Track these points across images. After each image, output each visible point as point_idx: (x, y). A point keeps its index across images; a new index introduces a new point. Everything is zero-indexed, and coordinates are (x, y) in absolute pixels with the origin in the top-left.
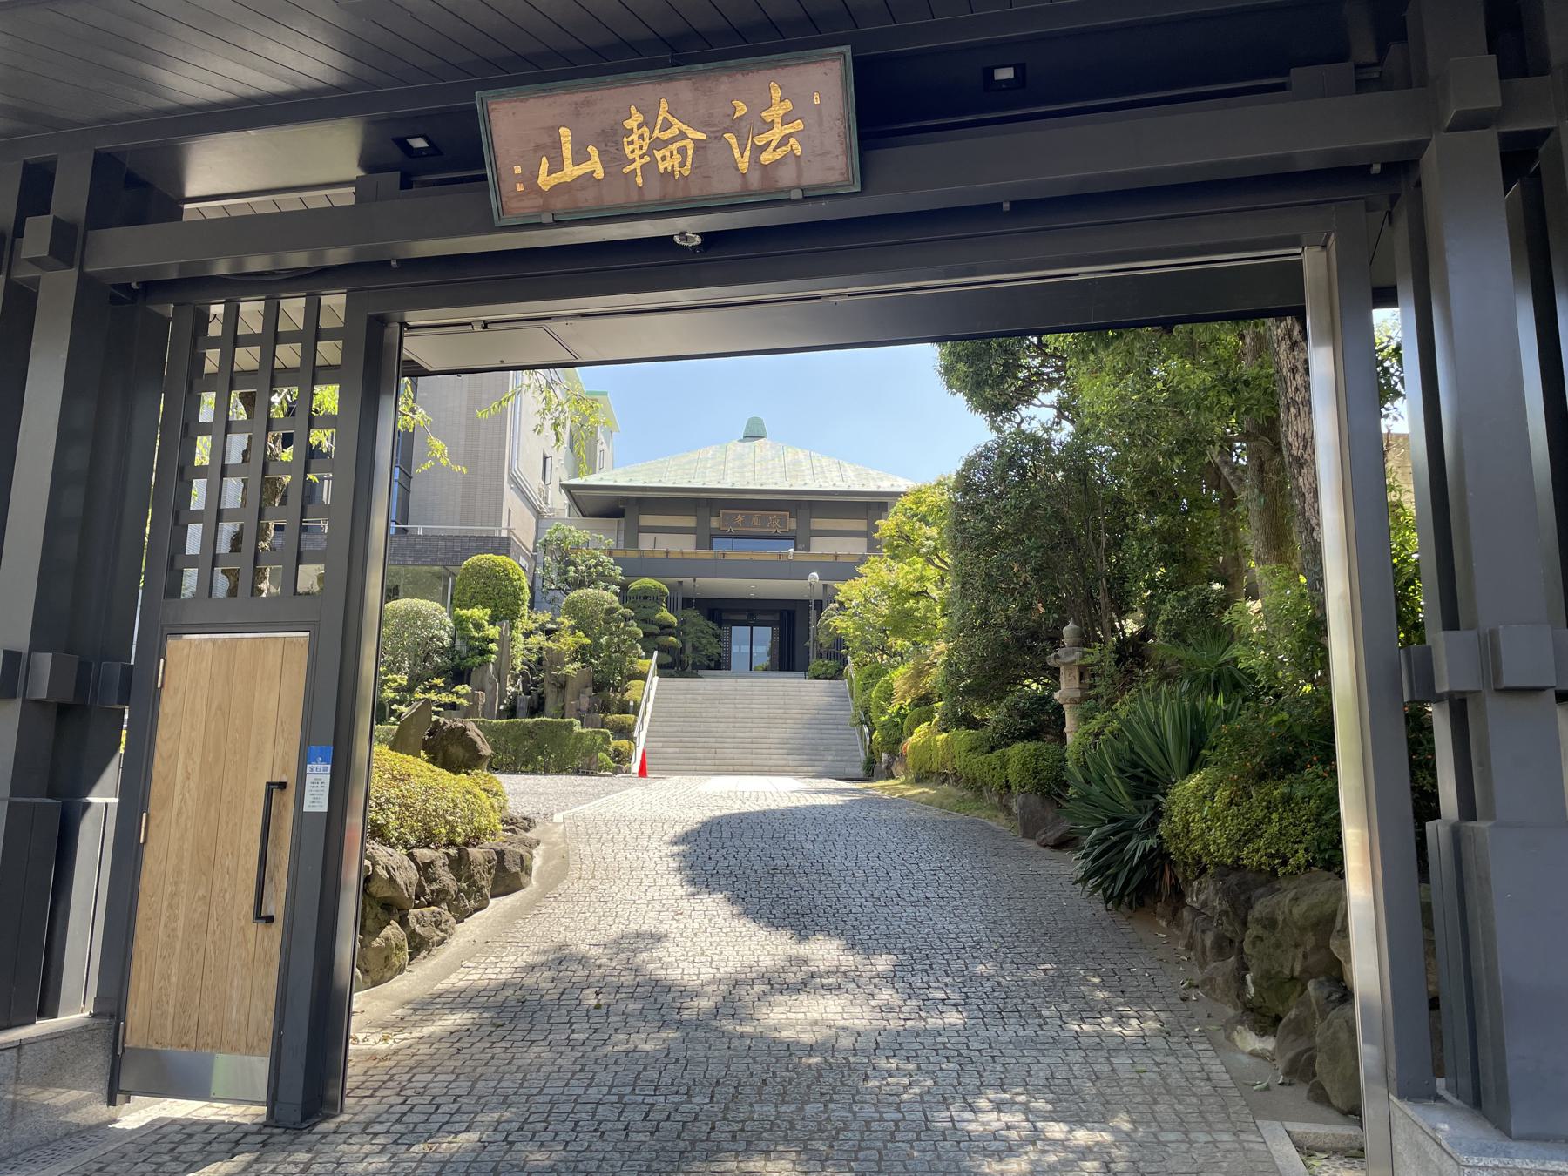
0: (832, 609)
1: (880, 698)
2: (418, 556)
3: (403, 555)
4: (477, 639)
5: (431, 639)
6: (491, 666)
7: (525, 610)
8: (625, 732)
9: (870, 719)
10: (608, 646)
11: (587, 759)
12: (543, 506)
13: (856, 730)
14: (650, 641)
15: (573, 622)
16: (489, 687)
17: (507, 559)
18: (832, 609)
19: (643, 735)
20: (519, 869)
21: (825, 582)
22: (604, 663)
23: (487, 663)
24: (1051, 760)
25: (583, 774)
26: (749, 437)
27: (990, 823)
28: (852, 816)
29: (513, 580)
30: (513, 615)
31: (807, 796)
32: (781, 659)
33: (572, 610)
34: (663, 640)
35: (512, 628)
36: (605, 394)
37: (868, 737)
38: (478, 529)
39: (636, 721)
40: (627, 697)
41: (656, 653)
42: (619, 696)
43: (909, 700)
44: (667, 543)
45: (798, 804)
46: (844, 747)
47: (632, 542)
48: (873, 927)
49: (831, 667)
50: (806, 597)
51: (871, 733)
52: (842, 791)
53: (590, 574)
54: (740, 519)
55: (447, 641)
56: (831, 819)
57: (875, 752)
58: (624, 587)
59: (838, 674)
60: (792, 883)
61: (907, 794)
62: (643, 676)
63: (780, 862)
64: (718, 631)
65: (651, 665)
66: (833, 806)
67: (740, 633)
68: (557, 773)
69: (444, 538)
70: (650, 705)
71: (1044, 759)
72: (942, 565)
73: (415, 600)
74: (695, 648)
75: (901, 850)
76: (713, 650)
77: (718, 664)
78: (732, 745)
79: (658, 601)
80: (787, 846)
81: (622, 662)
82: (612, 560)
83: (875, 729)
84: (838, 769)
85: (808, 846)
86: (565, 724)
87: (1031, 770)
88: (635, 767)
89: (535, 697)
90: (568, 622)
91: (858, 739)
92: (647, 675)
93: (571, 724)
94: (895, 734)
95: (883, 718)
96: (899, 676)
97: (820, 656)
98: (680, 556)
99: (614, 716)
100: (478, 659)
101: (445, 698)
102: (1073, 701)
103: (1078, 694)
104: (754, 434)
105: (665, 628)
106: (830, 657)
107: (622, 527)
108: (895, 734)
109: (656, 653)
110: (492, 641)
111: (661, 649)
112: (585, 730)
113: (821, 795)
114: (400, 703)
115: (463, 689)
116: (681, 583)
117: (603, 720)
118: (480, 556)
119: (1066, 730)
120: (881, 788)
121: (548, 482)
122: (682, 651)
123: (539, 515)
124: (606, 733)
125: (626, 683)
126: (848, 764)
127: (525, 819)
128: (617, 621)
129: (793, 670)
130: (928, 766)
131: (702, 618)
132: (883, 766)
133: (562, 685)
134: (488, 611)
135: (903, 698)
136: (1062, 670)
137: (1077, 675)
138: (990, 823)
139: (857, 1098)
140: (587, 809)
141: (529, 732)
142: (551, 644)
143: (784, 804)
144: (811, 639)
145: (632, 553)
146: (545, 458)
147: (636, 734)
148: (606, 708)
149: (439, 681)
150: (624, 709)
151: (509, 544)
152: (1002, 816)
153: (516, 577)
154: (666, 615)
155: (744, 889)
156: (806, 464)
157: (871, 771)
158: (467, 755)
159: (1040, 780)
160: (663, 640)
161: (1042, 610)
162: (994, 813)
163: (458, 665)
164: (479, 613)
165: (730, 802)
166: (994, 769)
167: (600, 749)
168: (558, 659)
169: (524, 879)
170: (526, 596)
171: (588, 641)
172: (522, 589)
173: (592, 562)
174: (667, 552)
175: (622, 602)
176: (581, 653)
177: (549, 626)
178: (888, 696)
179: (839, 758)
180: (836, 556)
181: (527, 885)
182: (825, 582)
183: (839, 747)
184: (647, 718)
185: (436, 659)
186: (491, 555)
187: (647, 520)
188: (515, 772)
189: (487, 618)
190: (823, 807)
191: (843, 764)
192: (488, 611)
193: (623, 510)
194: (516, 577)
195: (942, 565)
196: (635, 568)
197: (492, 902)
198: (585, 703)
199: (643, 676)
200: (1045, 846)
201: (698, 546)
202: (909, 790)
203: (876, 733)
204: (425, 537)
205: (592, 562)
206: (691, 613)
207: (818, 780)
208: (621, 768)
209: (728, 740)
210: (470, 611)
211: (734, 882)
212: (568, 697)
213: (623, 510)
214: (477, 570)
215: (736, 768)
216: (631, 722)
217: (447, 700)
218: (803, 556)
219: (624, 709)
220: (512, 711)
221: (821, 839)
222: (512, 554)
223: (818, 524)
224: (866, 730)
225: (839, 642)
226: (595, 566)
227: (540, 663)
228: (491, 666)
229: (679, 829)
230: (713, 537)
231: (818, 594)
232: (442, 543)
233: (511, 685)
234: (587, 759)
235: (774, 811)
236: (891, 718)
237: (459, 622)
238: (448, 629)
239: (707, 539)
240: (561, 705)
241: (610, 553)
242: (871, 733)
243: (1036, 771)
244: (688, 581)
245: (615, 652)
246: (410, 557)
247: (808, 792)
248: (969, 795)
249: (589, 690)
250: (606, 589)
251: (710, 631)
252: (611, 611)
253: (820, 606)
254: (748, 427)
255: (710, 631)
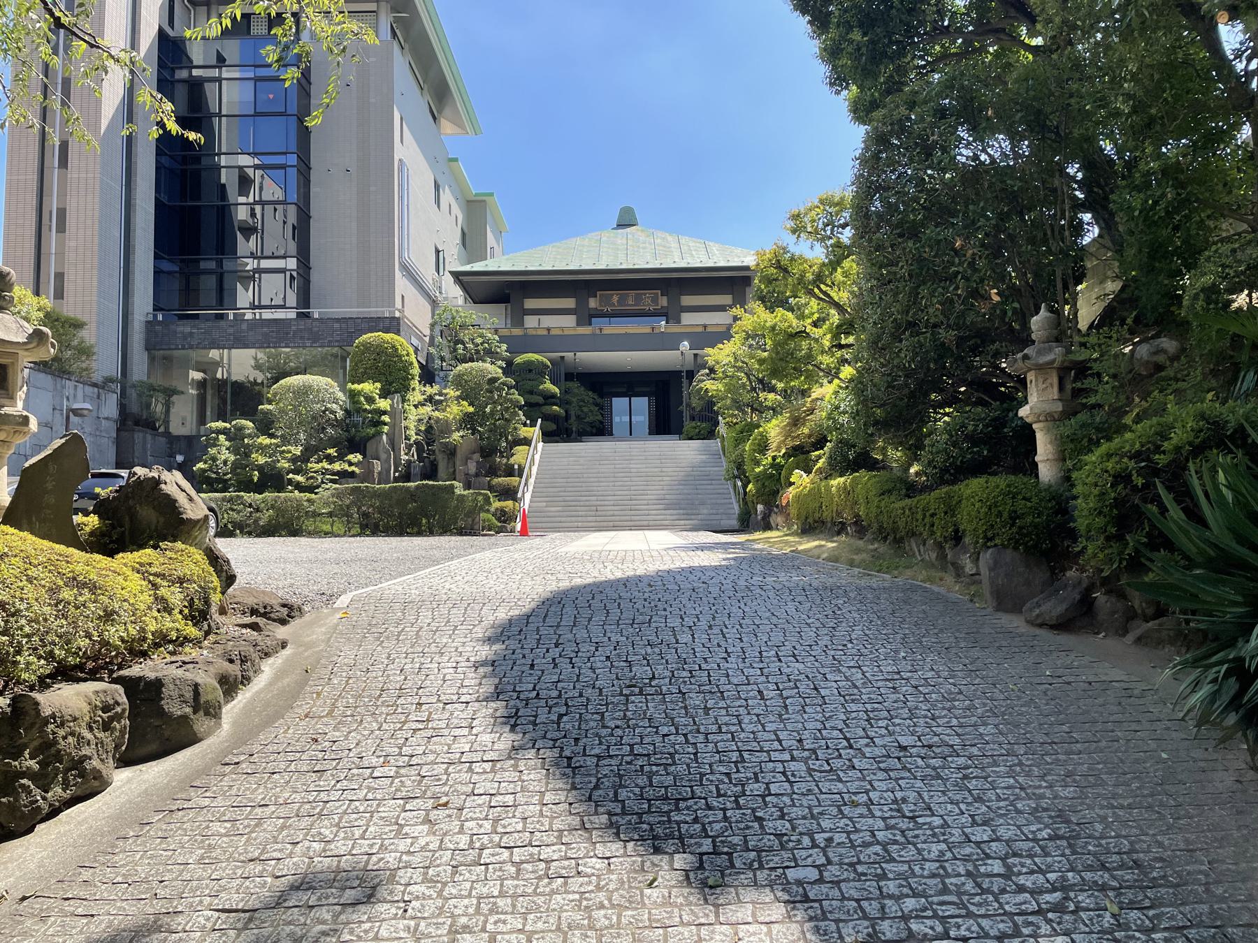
0: (702, 375)
1: (754, 450)
2: (315, 338)
3: (302, 338)
4: (370, 412)
5: (324, 412)
6: (384, 437)
7: (415, 383)
8: (510, 493)
9: (744, 473)
10: (493, 412)
11: (470, 520)
12: (438, 294)
13: (729, 485)
14: (533, 410)
15: (458, 393)
16: (383, 456)
17: (396, 337)
18: (702, 375)
19: (528, 497)
20: (188, 710)
21: (696, 352)
22: (490, 431)
23: (380, 433)
24: (1035, 500)
25: (466, 535)
26: (621, 226)
27: (935, 588)
28: (742, 583)
29: (400, 356)
30: (404, 388)
31: (683, 554)
32: (657, 426)
33: (459, 382)
34: (546, 409)
35: (404, 401)
36: (492, 195)
37: (741, 491)
38: (373, 311)
39: (520, 483)
40: (512, 460)
41: (540, 420)
42: (505, 460)
43: (783, 451)
44: (549, 321)
45: (672, 566)
46: (719, 501)
47: (519, 323)
48: (820, 838)
49: (703, 428)
50: (678, 368)
51: (745, 486)
52: (725, 546)
53: (477, 352)
54: (615, 298)
55: (340, 414)
56: (715, 590)
57: (750, 504)
58: (510, 363)
59: (710, 434)
60: (659, 717)
61: (801, 548)
62: (527, 442)
63: (641, 671)
64: (599, 400)
65: (535, 432)
66: (716, 568)
67: (619, 403)
68: (441, 534)
69: (338, 320)
70: (535, 469)
71: (1024, 498)
72: (821, 296)
73: (308, 376)
74: (578, 417)
75: (825, 640)
76: (593, 416)
77: (601, 430)
78: (612, 503)
79: (542, 374)
80: (653, 638)
81: (505, 428)
82: (497, 338)
83: (749, 482)
84: (715, 522)
85: (685, 638)
86: (446, 487)
87: (1005, 515)
88: (519, 527)
89: (427, 464)
90: (452, 392)
91: (732, 491)
92: (531, 441)
93: (452, 487)
94: (774, 483)
95: (757, 470)
96: (774, 429)
97: (693, 418)
98: (560, 333)
99: (500, 479)
100: (372, 431)
101: (337, 466)
102: (1050, 418)
103: (1059, 407)
104: (626, 221)
105: (549, 398)
106: (702, 419)
107: (509, 312)
108: (771, 485)
109: (540, 420)
110: (385, 413)
111: (546, 418)
112: (466, 492)
113: (699, 553)
114: (296, 472)
115: (356, 457)
116: (562, 358)
117: (489, 482)
118: (370, 335)
119: (1037, 459)
120: (763, 541)
121: (441, 273)
122: (567, 417)
123: (434, 303)
124: (486, 495)
125: (511, 449)
126: (724, 517)
127: (284, 606)
128: (500, 389)
129: (669, 433)
130: (817, 515)
131: (582, 389)
132: (759, 517)
133: (451, 452)
134: (378, 385)
135: (778, 449)
136: (1031, 376)
137: (1055, 380)
138: (935, 588)
139: (742, 801)
140: (392, 587)
141: (412, 495)
142: (437, 414)
143: (652, 567)
144: (684, 404)
145: (517, 332)
146: (438, 252)
147: (519, 495)
148: (493, 471)
149: (331, 451)
150: (510, 472)
151: (399, 324)
152: (949, 579)
153: (405, 352)
154: (549, 386)
155: (575, 734)
156: (674, 245)
157: (746, 523)
158: (162, 520)
159: (1021, 528)
160: (546, 409)
161: (996, 298)
162: (933, 573)
163: (354, 437)
164: (368, 387)
165: (589, 566)
166: (933, 515)
167: (482, 509)
168: (446, 428)
169: (201, 724)
170: (416, 371)
171: (471, 409)
172: (411, 364)
173: (479, 340)
174: (549, 330)
175: (504, 373)
176: (468, 421)
177: (437, 397)
178: (763, 447)
179: (714, 511)
180: (705, 326)
181: (209, 733)
182: (696, 352)
183: (714, 501)
184: (532, 481)
185: (330, 430)
186: (380, 333)
187: (530, 303)
188: (401, 535)
189: (377, 391)
190: (703, 569)
191: (718, 517)
192: (378, 385)
193: (509, 295)
194: (405, 352)
195: (821, 296)
196: (517, 346)
197: (122, 778)
198: (472, 467)
199: (527, 442)
200: (1041, 626)
201: (579, 324)
202: (800, 543)
203: (750, 486)
204: (320, 320)
205: (479, 340)
206: (574, 385)
207: (695, 533)
208: (506, 527)
209: (610, 498)
210: (362, 385)
211: (561, 716)
212: (458, 463)
213: (509, 295)
214: (367, 347)
215: (616, 523)
216: (516, 484)
217: (339, 468)
218: (674, 329)
219: (510, 472)
220: (407, 477)
221: (703, 624)
222: (402, 333)
223: (687, 300)
224: (739, 484)
225: (710, 404)
226: (482, 344)
227: (431, 432)
228: (384, 437)
229: (502, 615)
230: (592, 316)
231: (689, 363)
232: (337, 325)
233: (406, 454)
234: (470, 520)
235: (640, 579)
236: (765, 470)
237: (353, 395)
238: (341, 403)
239: (583, 317)
240: (451, 470)
241: (496, 331)
242: (745, 486)
243: (1014, 516)
244: (568, 356)
245: (499, 419)
246: (308, 339)
247: (686, 548)
248: (882, 548)
249: (477, 456)
250: (493, 363)
251: (591, 401)
252: (493, 380)
253: (691, 375)
254: (620, 216)
255: (591, 401)
